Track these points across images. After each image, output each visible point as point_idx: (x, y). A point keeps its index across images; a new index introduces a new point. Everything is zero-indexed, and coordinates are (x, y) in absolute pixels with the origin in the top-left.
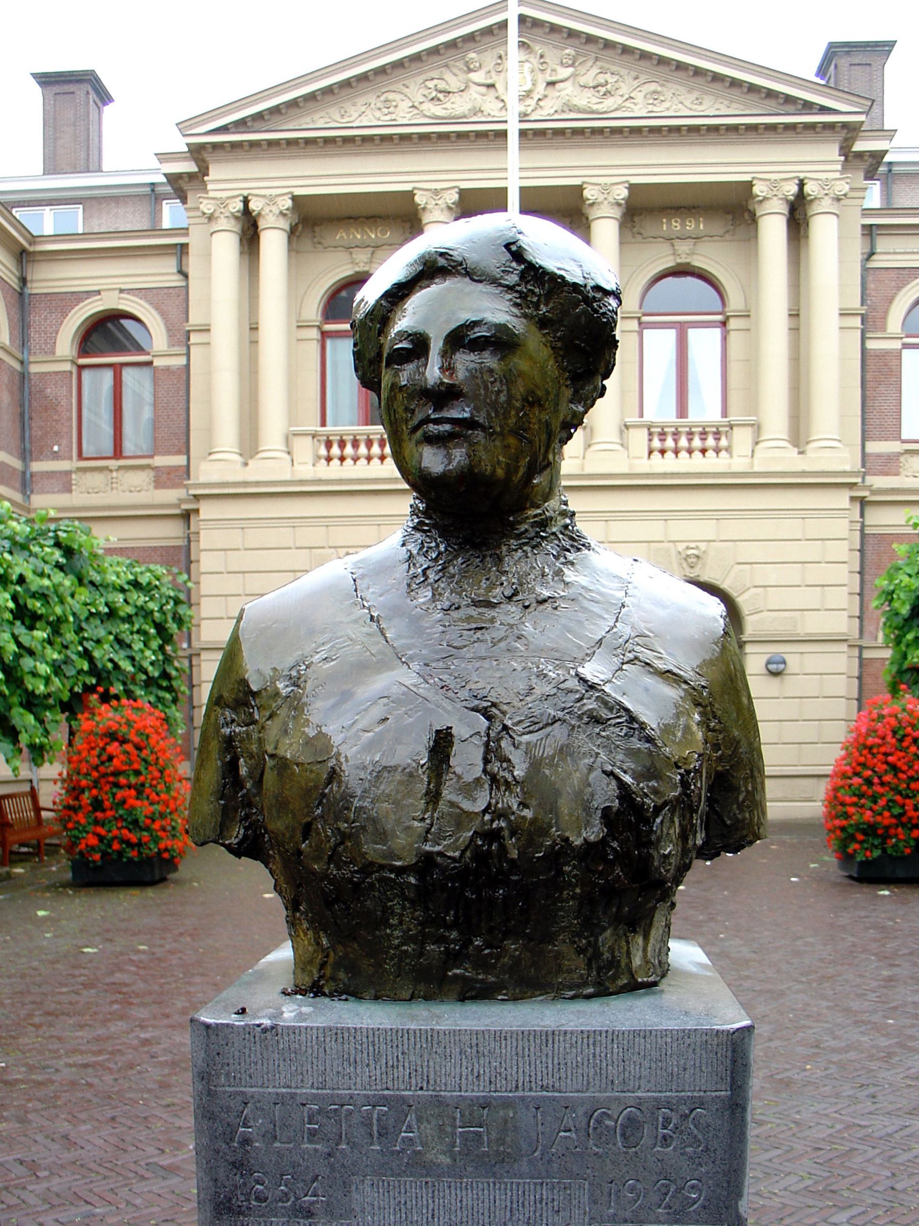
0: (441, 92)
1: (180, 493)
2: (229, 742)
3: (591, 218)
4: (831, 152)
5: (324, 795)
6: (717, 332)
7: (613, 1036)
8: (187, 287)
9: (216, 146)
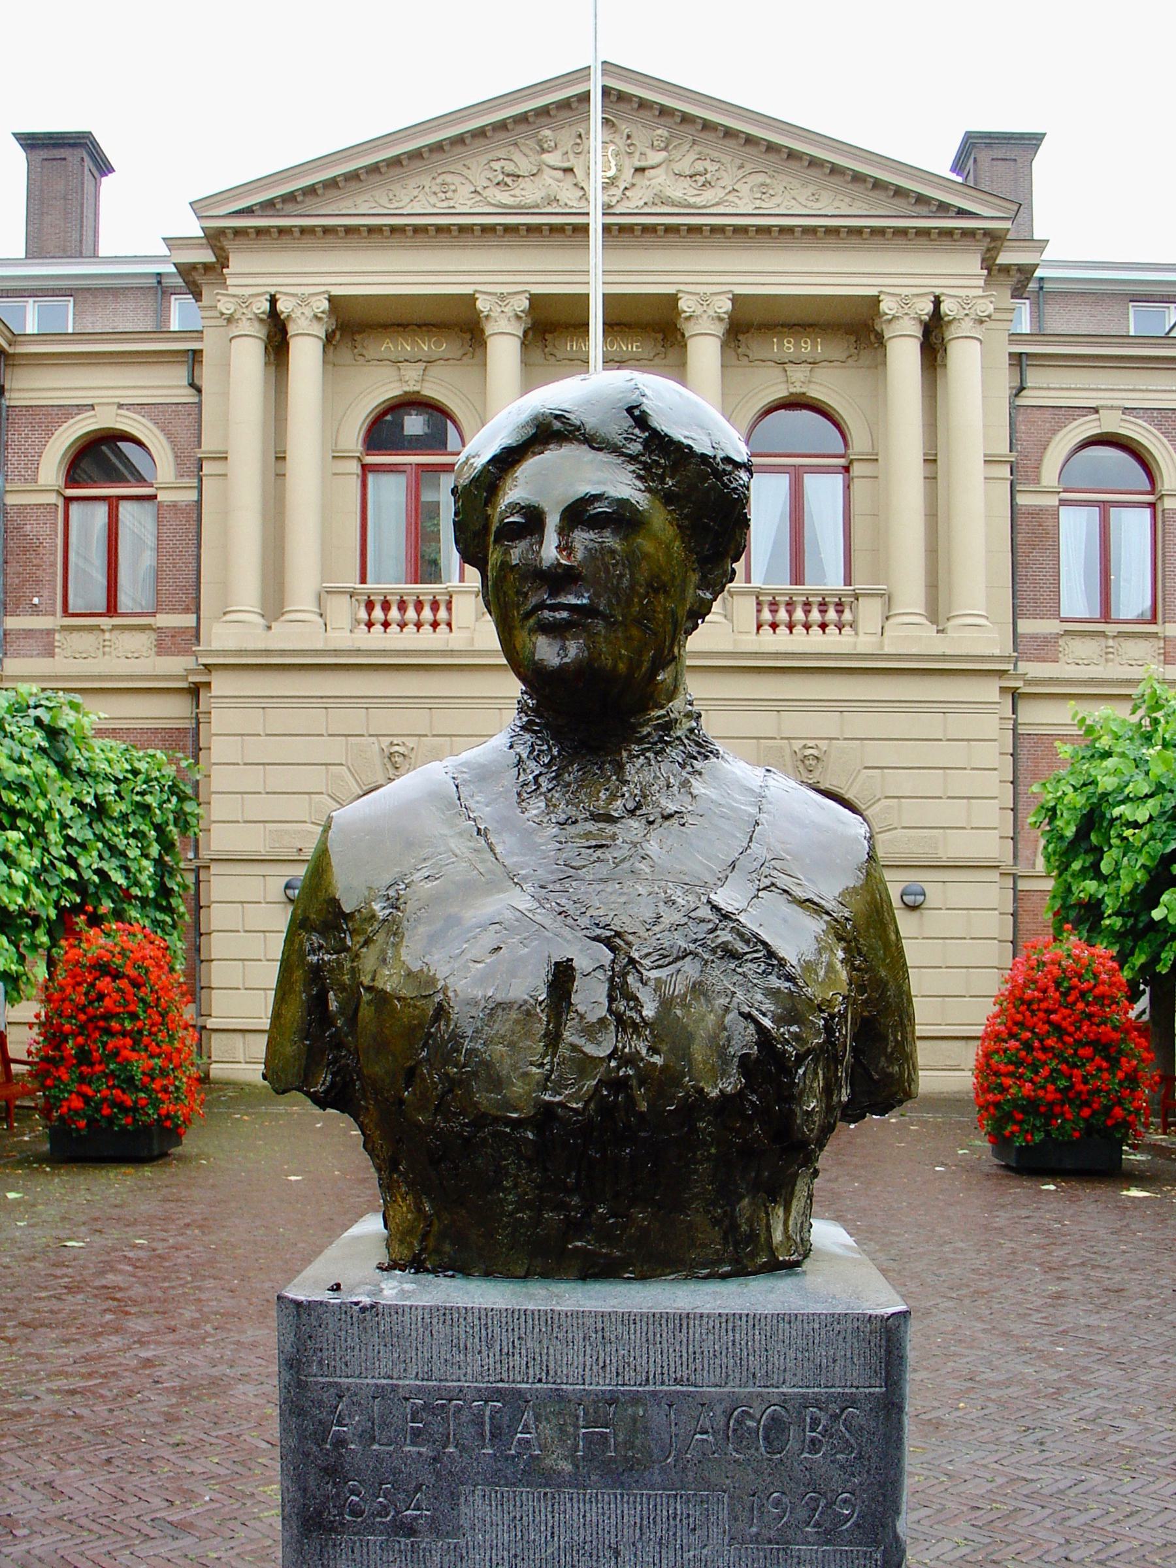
0: (508, 175)
1: (187, 662)
2: (316, 971)
3: (687, 335)
4: (970, 264)
5: (430, 1035)
6: (837, 481)
7: (754, 1320)
8: (199, 405)
9: (238, 232)
